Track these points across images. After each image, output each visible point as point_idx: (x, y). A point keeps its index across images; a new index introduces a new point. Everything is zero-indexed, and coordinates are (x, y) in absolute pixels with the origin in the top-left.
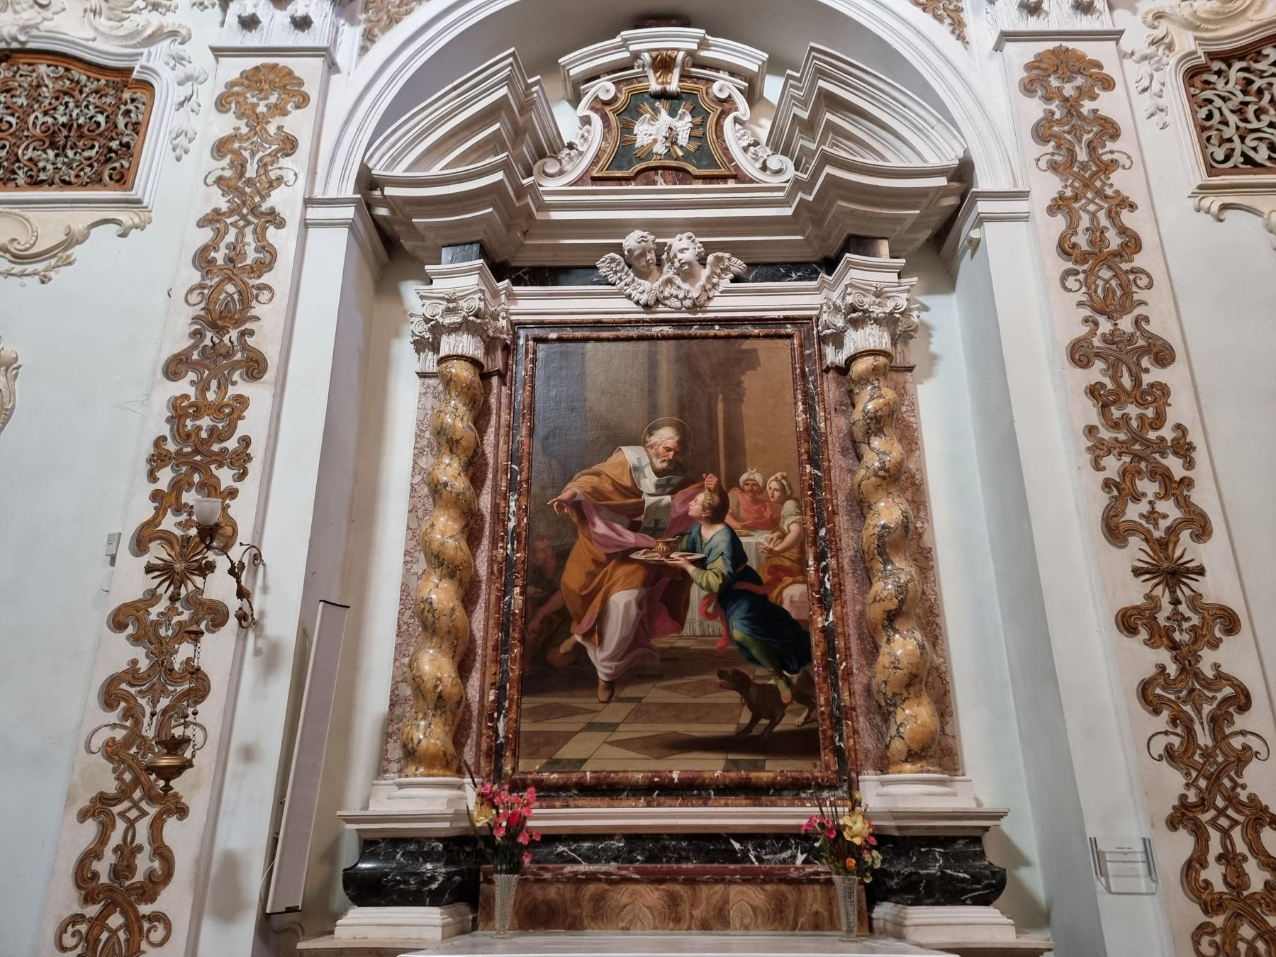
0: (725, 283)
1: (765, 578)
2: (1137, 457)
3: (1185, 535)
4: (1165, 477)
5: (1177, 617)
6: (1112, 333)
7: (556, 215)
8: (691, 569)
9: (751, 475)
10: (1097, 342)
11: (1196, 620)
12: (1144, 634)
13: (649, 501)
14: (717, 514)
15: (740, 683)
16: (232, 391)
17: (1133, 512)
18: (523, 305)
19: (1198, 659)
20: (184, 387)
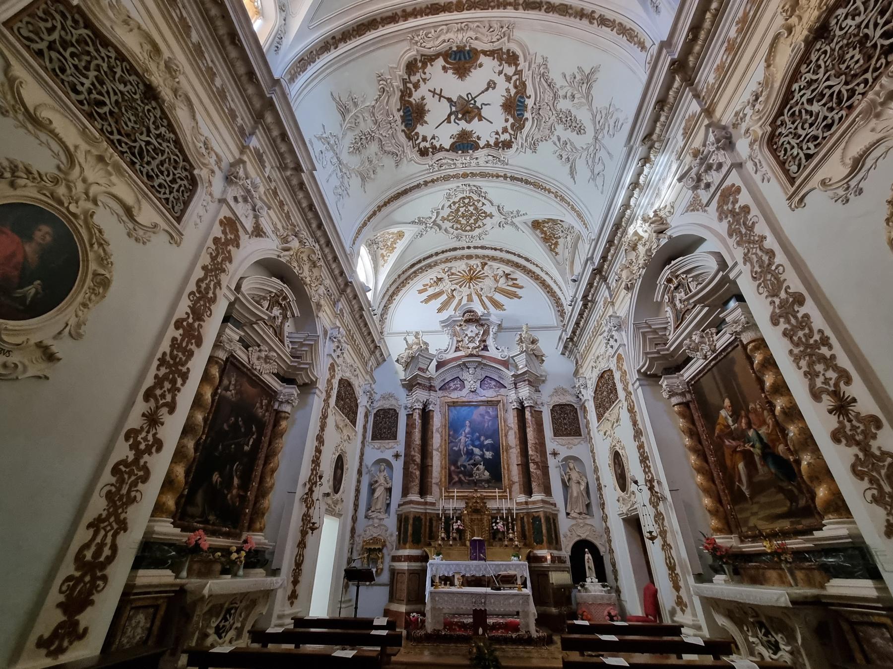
0: (715, 338)
1: (770, 444)
2: (811, 355)
3: (842, 384)
4: (822, 359)
5: (854, 428)
6: (781, 303)
7: (672, 349)
8: (752, 449)
9: (751, 406)
10: (777, 311)
11: (862, 427)
12: (844, 441)
13: (733, 427)
14: (749, 425)
15: (781, 490)
16: (800, 315)
17: (819, 382)
18: (686, 376)
19: (870, 446)
20: (783, 325)
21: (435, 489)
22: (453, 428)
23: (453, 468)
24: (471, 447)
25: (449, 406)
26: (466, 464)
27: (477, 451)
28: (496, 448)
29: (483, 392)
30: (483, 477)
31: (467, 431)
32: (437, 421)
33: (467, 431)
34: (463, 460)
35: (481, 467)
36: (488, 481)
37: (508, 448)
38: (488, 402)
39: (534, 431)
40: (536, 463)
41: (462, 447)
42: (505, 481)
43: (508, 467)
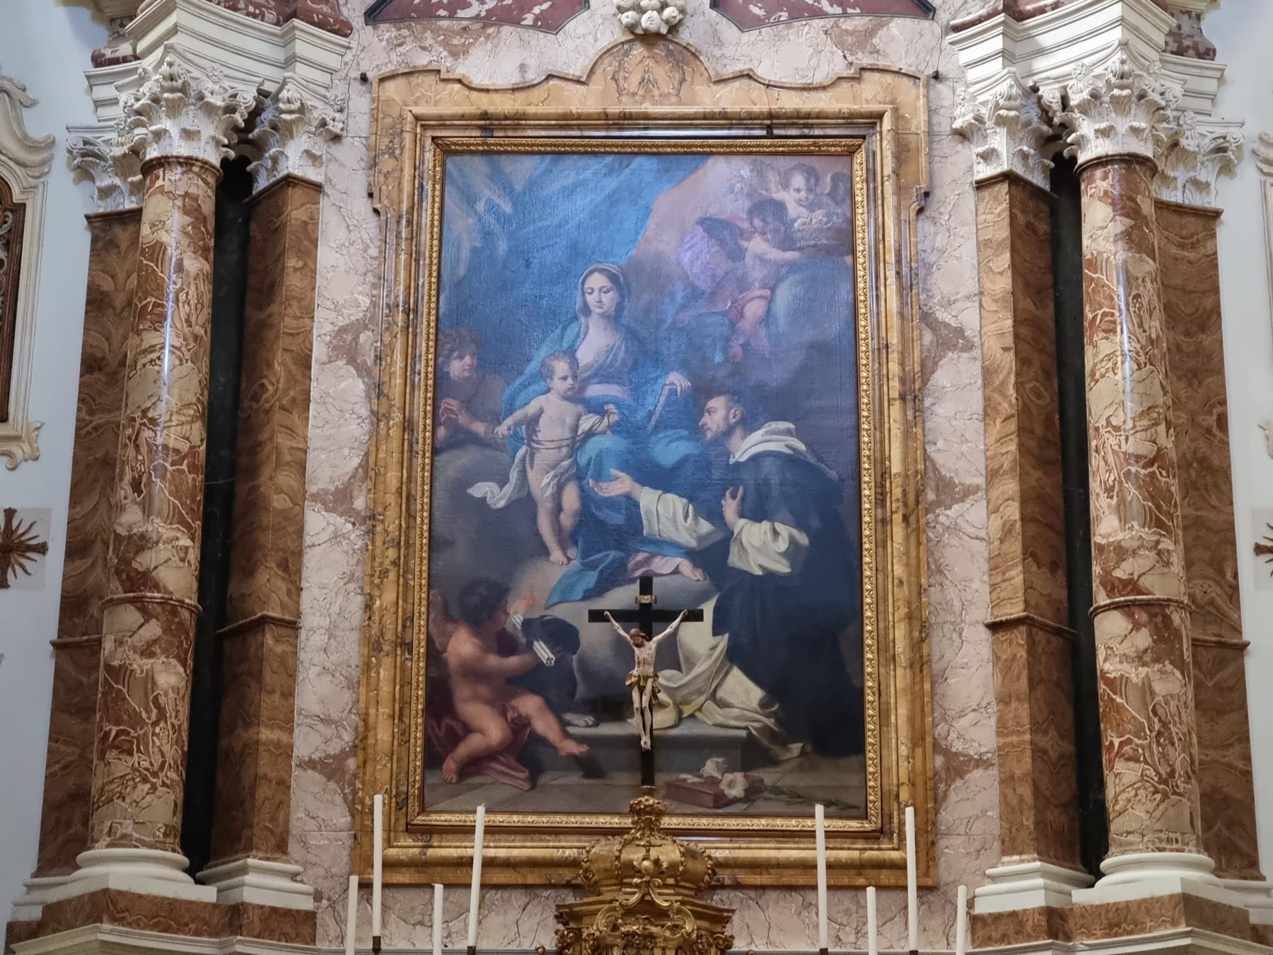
21: (315, 808)
22: (472, 329)
23: (462, 645)
24: (619, 485)
25: (446, 150)
26: (574, 613)
27: (667, 513)
28: (826, 502)
29: (740, 48)
30: (711, 722)
31: (587, 354)
32: (344, 271)
33: (587, 354)
34: (546, 585)
35: (700, 639)
36: (748, 752)
37: (925, 493)
38: (772, 122)
39: (1145, 358)
40: (1153, 612)
41: (542, 484)
42: (890, 752)
43: (918, 644)
